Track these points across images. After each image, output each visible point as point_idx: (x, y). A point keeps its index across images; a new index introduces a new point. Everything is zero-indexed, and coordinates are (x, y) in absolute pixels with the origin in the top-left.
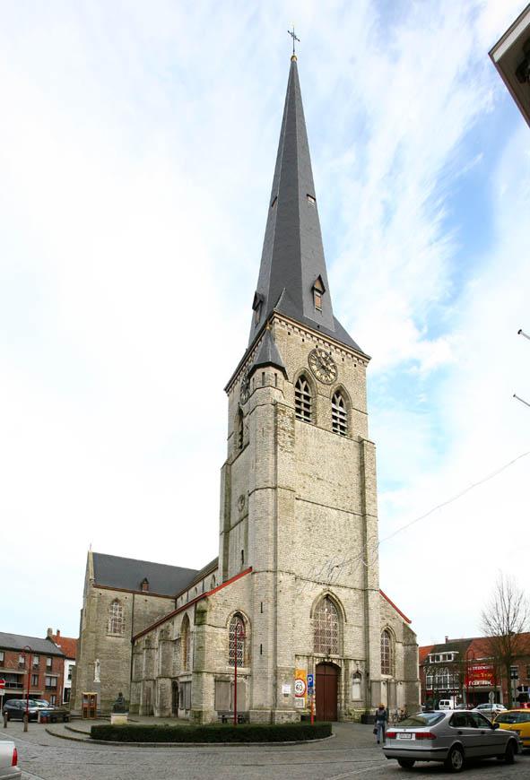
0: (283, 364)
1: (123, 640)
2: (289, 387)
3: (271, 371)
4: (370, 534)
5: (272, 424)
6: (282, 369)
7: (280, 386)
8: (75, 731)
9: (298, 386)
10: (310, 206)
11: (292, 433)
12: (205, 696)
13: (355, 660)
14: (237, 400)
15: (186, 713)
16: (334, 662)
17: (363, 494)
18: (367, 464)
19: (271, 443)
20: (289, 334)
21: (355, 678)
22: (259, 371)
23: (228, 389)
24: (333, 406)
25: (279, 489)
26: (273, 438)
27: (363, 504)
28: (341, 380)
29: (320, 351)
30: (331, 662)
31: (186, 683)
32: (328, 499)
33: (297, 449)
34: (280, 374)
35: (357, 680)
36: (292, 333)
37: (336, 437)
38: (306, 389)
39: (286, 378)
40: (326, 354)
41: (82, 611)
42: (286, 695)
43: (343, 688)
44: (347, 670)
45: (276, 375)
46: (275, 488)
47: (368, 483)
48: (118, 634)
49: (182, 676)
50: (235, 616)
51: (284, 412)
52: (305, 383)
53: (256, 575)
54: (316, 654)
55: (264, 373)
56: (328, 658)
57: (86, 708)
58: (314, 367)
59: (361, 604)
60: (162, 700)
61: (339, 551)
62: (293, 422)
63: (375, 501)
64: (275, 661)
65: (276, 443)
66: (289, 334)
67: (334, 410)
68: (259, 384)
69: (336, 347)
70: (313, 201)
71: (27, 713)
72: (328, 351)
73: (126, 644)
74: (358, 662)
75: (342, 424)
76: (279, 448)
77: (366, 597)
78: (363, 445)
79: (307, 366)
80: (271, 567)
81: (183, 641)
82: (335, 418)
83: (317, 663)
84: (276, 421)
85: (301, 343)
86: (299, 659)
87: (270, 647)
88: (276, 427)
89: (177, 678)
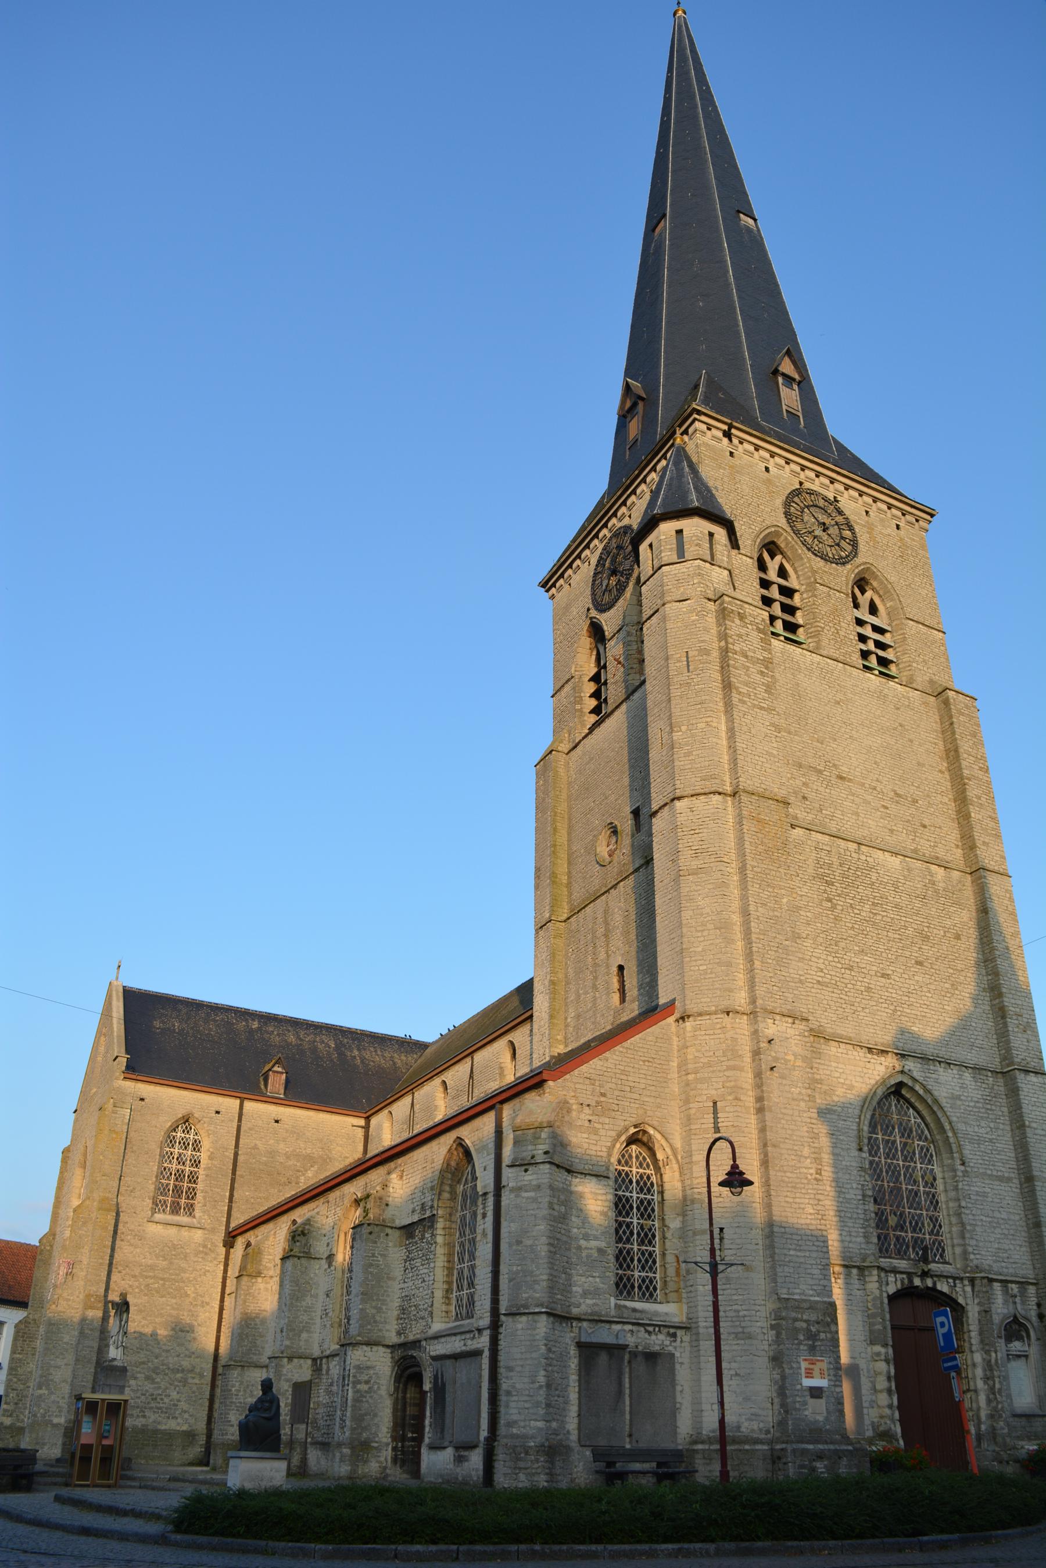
0: (728, 512)
1: (198, 1235)
2: (744, 563)
3: (695, 527)
5: (714, 645)
6: (729, 527)
8: (123, 1513)
9: (762, 566)
10: (748, 230)
11: (768, 663)
13: (1004, 1282)
15: (459, 1460)
16: (943, 1287)
17: (963, 816)
18: (965, 746)
19: (717, 686)
20: (731, 454)
21: (1009, 1339)
22: (666, 528)
25: (744, 798)
26: (717, 676)
27: (968, 843)
30: (934, 1289)
31: (456, 1357)
32: (873, 825)
34: (720, 533)
35: (1016, 1346)
37: (873, 680)
38: (782, 573)
39: (734, 543)
41: (66, 1152)
42: (816, 1393)
43: (979, 1372)
44: (986, 1312)
45: (711, 535)
46: (734, 794)
47: (972, 791)
48: (183, 1219)
49: (436, 1337)
50: (632, 1141)
51: (742, 617)
52: (778, 558)
53: (689, 1024)
54: (884, 1262)
55: (680, 532)
56: (925, 1274)
57: (87, 1448)
59: (1002, 1109)
60: (358, 1419)
61: (919, 963)
63: (998, 836)
64: (773, 1278)
65: (727, 686)
67: (860, 622)
68: (669, 554)
69: (847, 487)
70: (751, 221)
71: (621, 1232)
73: (205, 1250)
74: (1014, 1288)
75: (881, 653)
77: (1013, 1092)
78: (946, 702)
80: (741, 1000)
81: (440, 1224)
82: (863, 639)
83: (892, 1289)
84: (723, 636)
88: (725, 652)
89: (416, 1344)
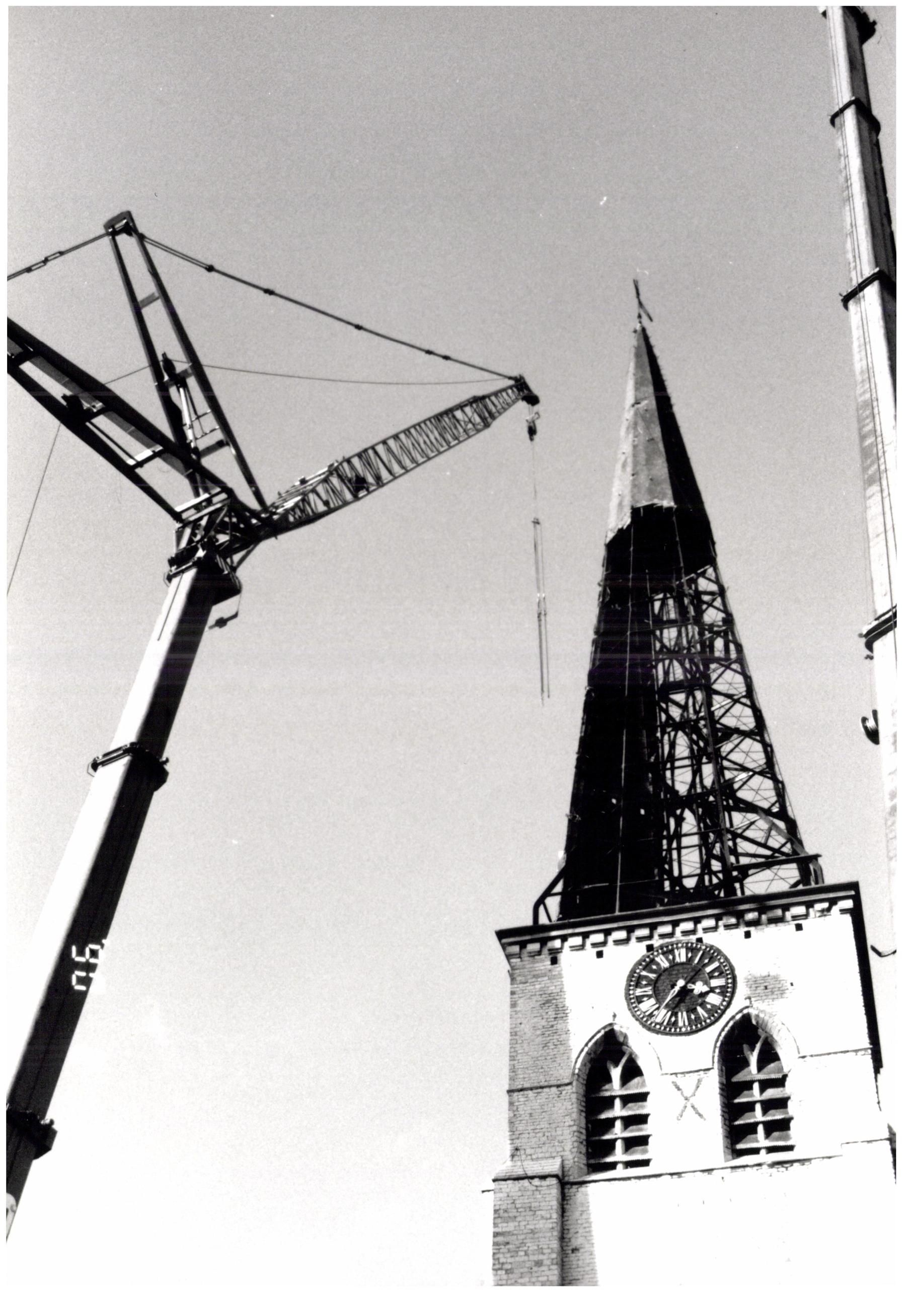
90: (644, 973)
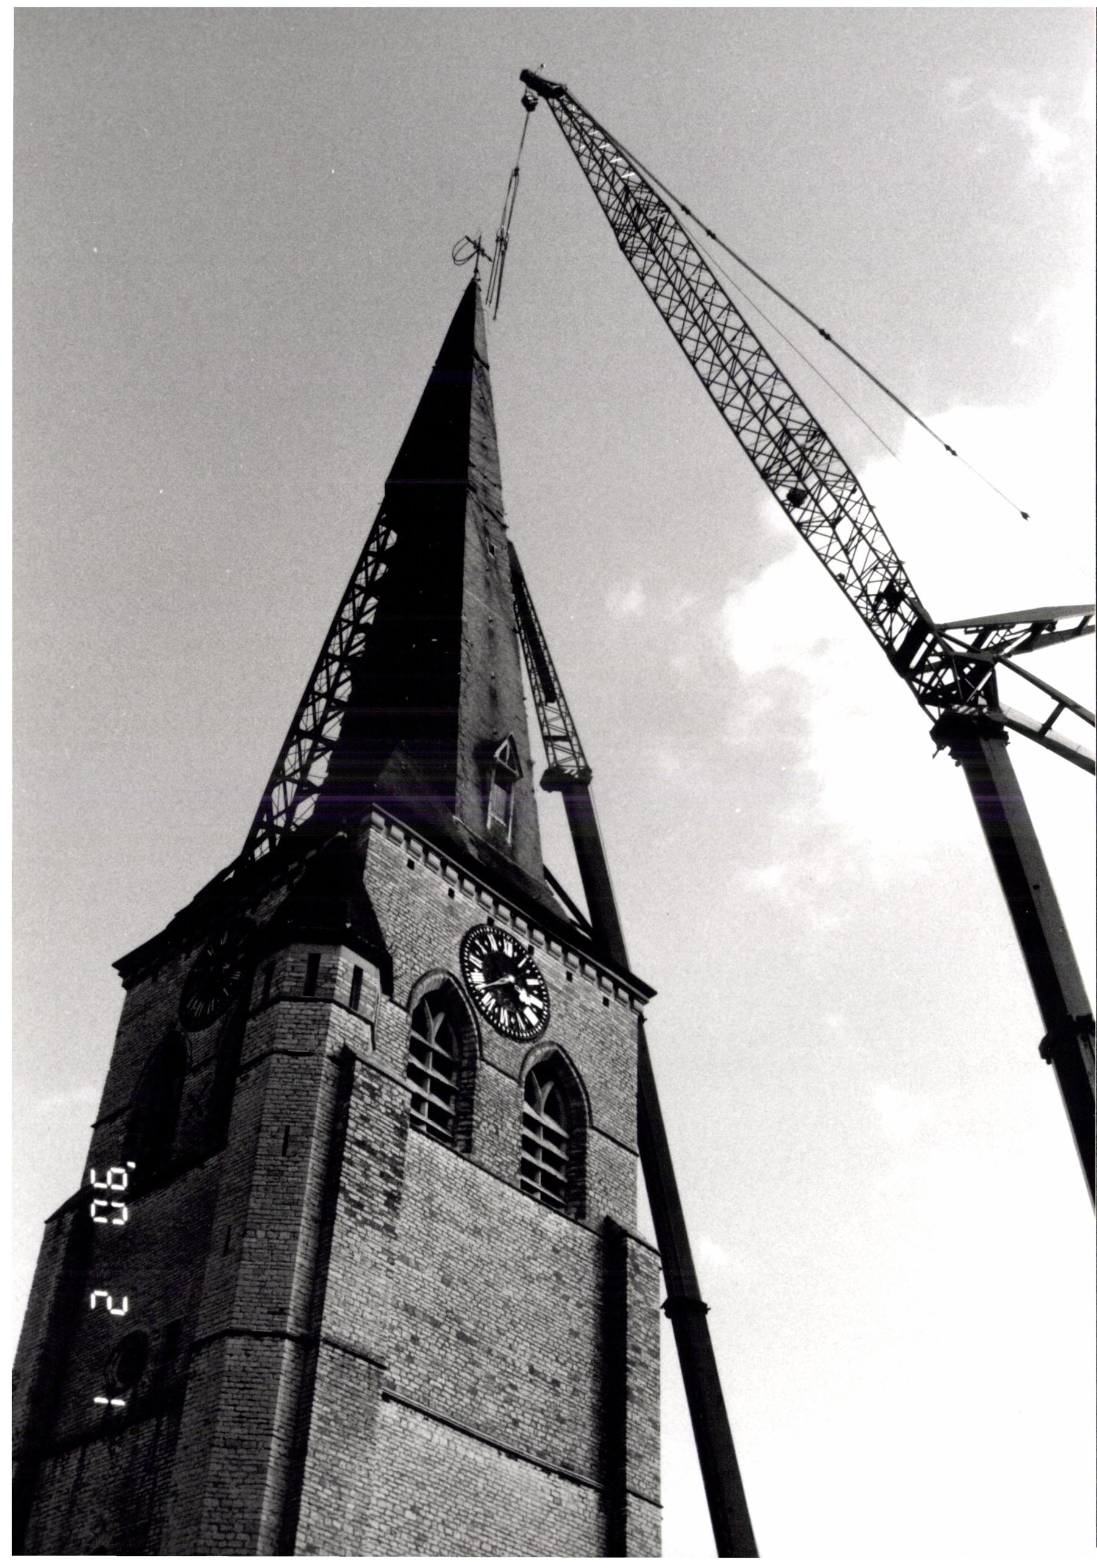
4: (1086, 715)
7: (366, 1007)
11: (397, 1168)
12: (300, 1314)
14: (165, 1009)
20: (411, 865)
23: (47, 1222)
24: (527, 1109)
28: (559, 1032)
29: (500, 936)
33: (407, 1220)
36: (419, 863)
40: (517, 947)
58: (477, 977)
62: (402, 1133)
66: (411, 865)
72: (525, 943)
76: (341, 1205)
79: (456, 970)
82: (528, 1145)
85: (445, 900)
86: (651, 1436)
87: (645, 1226)
90: (477, 942)
